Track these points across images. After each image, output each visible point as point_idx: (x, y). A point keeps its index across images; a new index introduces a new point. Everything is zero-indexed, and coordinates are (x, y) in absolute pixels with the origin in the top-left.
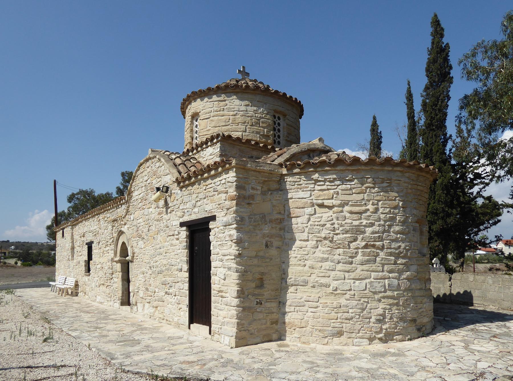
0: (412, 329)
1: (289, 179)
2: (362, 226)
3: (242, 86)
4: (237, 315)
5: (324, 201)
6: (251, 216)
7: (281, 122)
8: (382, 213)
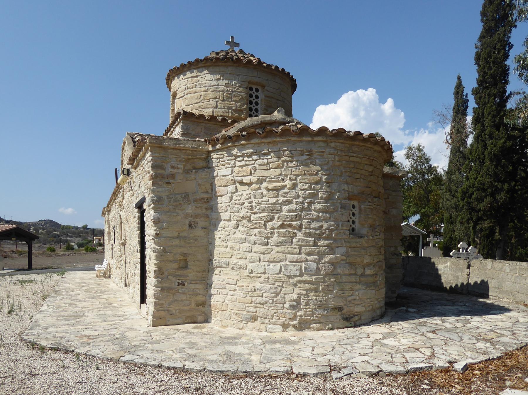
0: (337, 317)
1: (215, 156)
2: (278, 204)
3: (232, 58)
4: (155, 295)
5: (243, 178)
6: (171, 196)
7: (260, 94)
8: (301, 190)
